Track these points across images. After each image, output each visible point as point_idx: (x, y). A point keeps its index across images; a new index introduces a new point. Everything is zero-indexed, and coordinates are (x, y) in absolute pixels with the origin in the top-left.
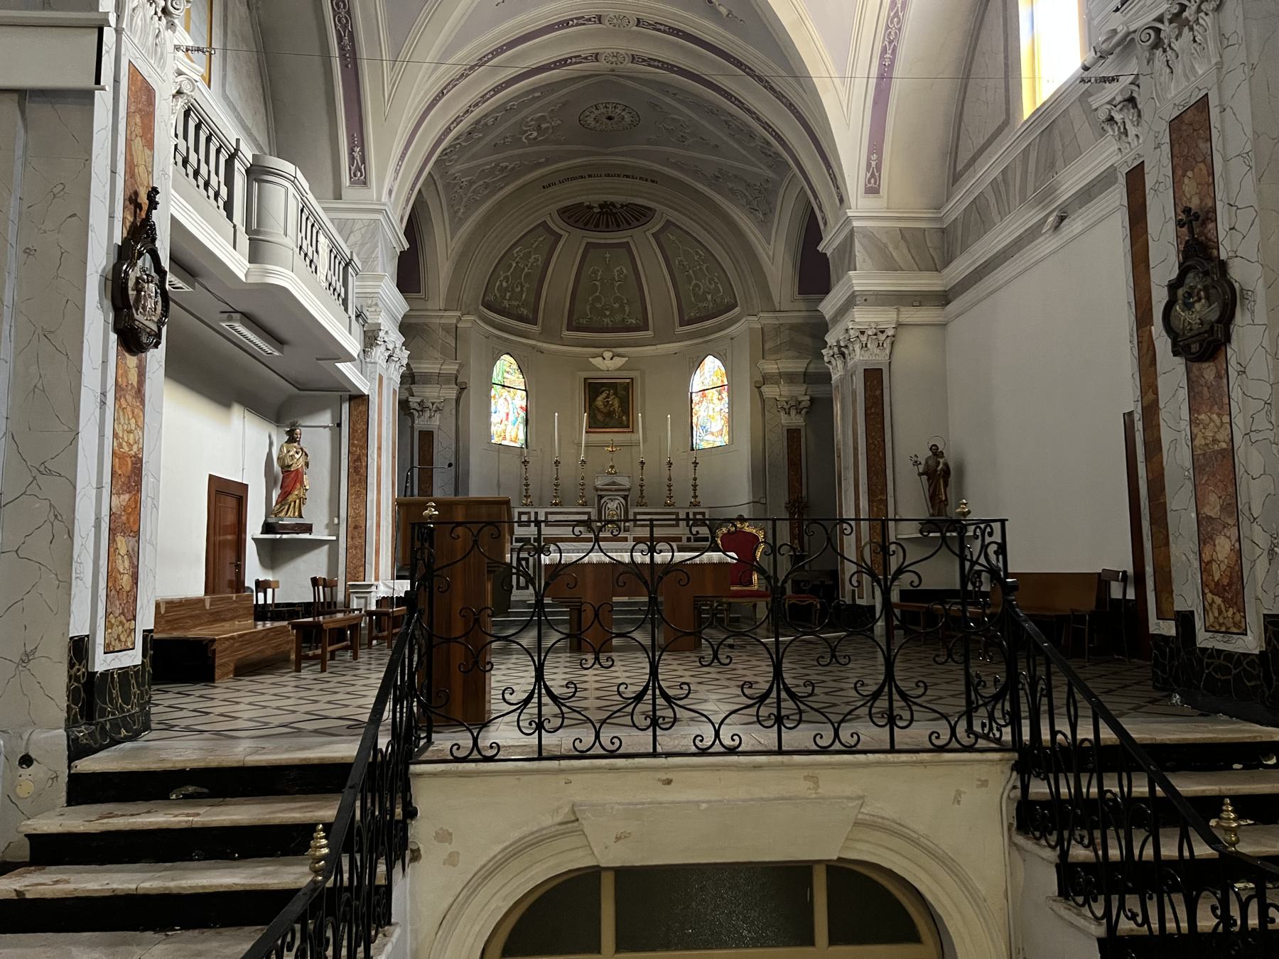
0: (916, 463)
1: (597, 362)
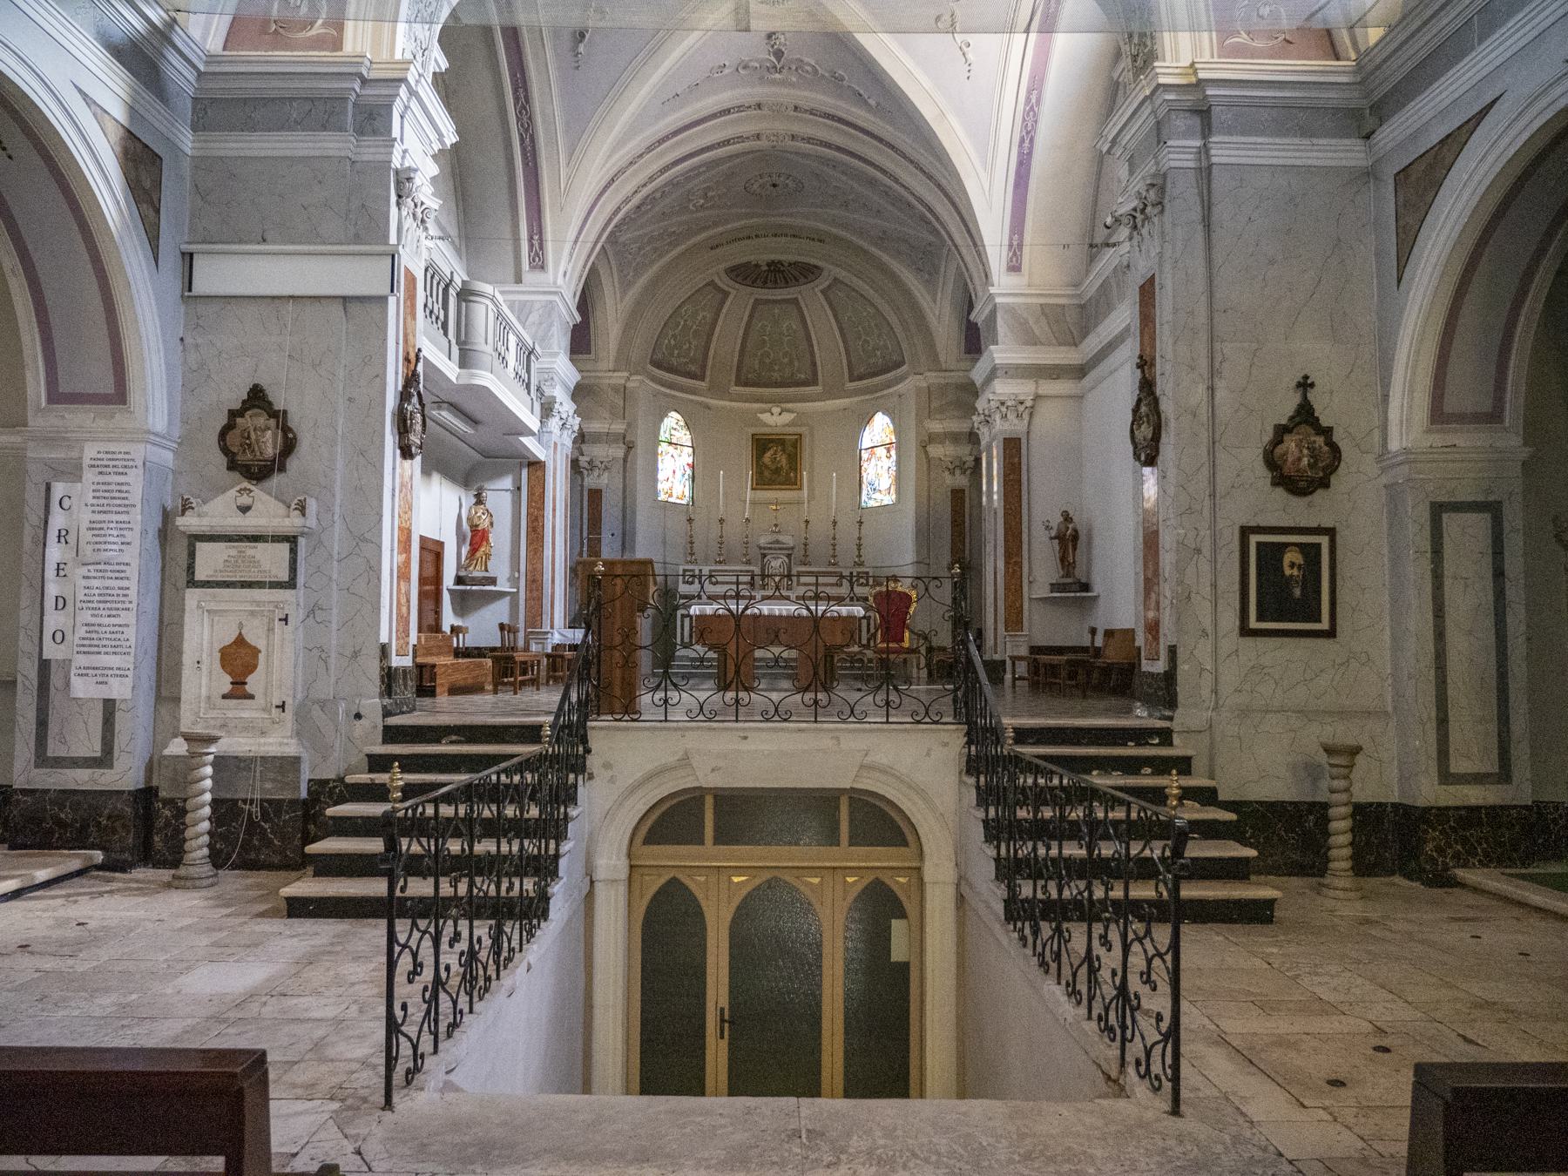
1: (765, 417)
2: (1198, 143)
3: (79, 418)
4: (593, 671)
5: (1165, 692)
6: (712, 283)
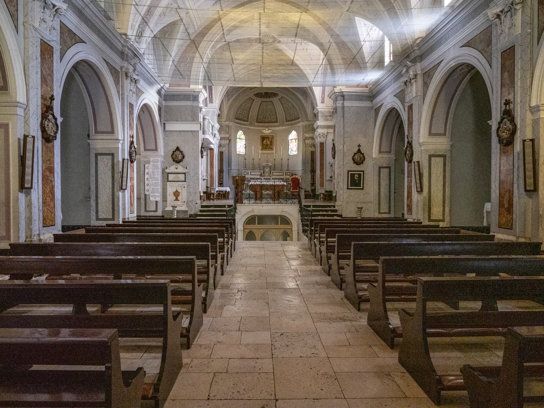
1: (264, 131)
3: (149, 153)
6: (250, 98)
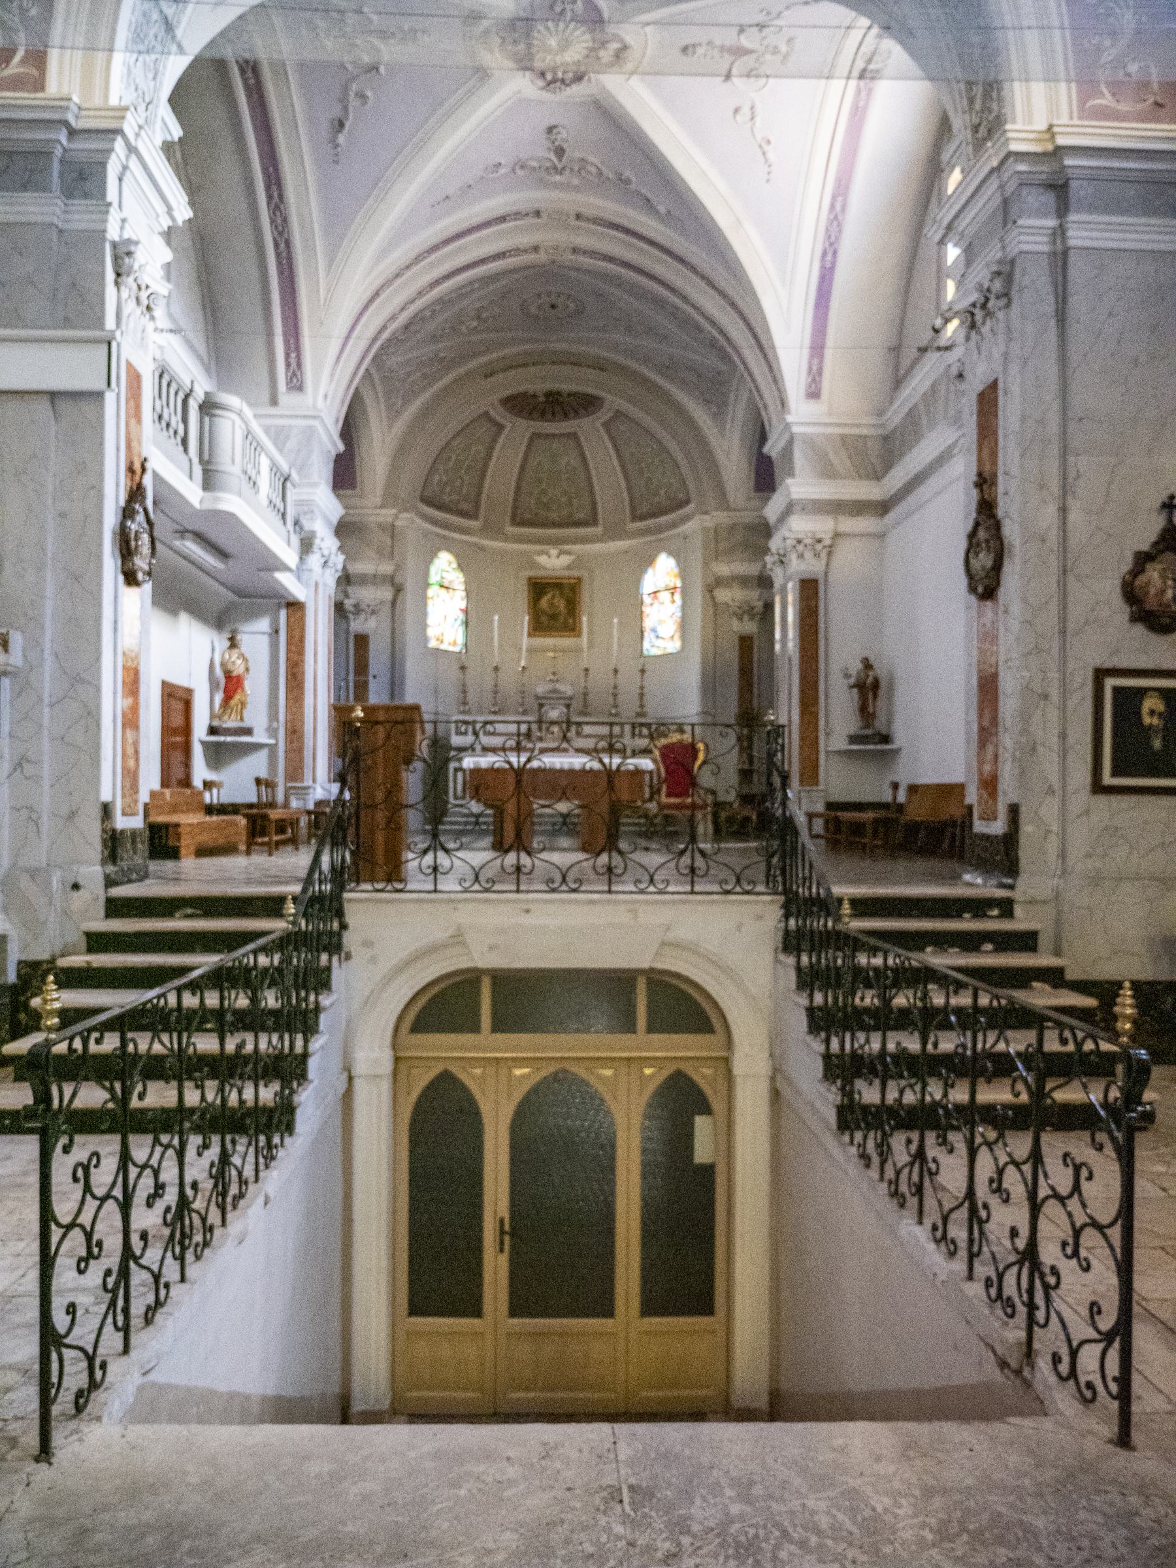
0: (847, 676)
2: (1052, 222)
4: (351, 831)
5: (1003, 856)
